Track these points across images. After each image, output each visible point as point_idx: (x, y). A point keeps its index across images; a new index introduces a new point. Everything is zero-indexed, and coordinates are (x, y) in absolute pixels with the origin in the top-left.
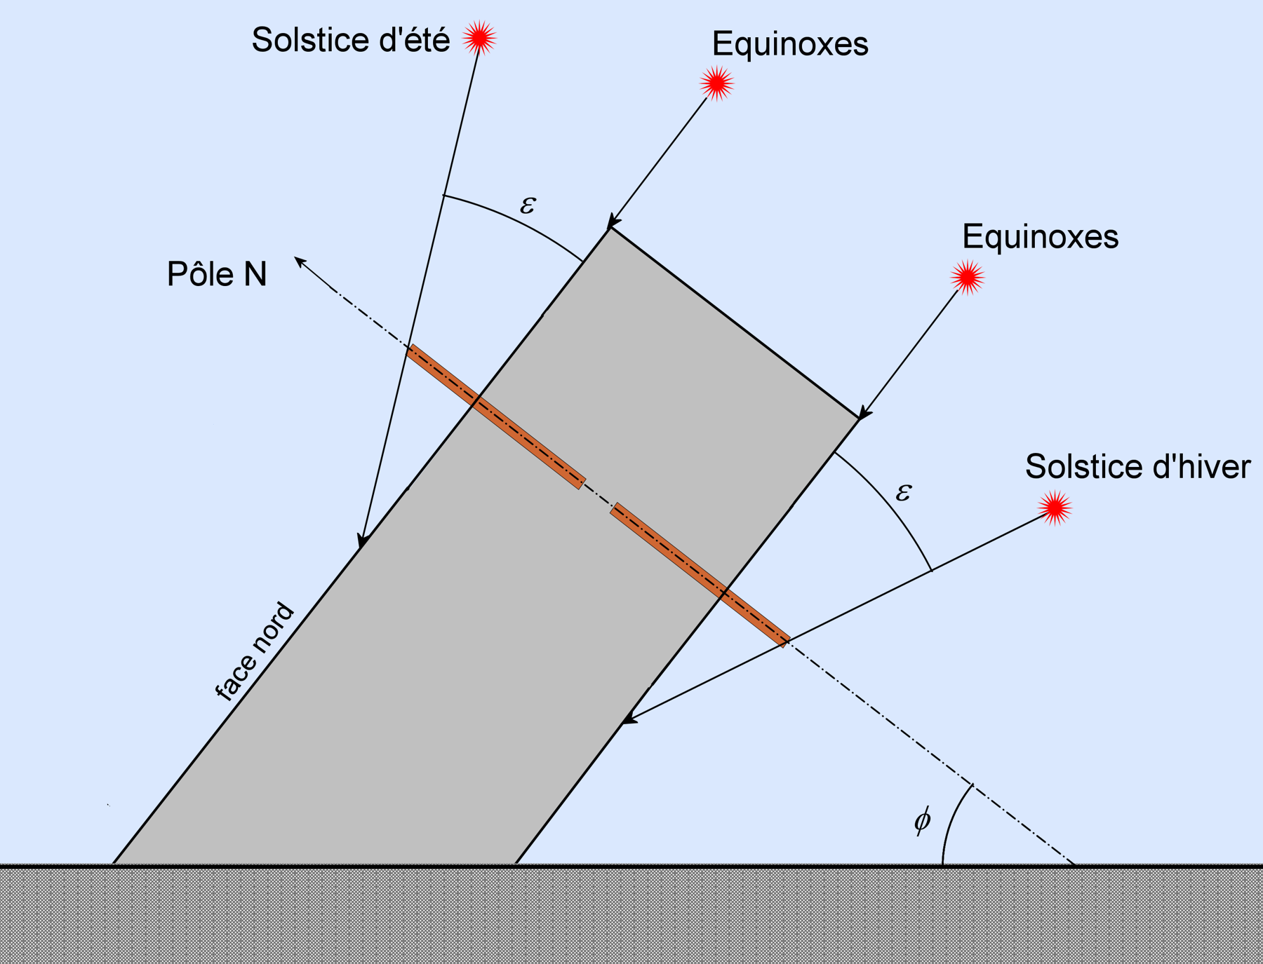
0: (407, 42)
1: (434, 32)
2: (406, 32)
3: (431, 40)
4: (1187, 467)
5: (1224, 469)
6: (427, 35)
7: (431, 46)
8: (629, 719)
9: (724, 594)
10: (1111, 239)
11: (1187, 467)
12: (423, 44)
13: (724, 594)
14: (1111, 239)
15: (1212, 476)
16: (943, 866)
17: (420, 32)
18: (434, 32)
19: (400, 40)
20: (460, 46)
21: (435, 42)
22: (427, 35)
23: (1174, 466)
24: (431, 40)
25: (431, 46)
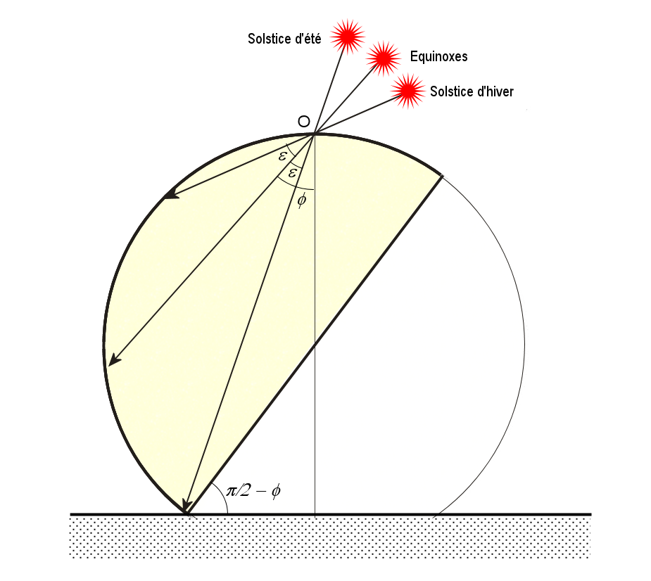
0: (306, 39)
1: (315, 35)
2: (305, 35)
3: (314, 39)
4: (490, 92)
5: (504, 92)
6: (313, 36)
7: (314, 41)
8: (171, 194)
9: (296, 187)
10: (254, 39)
11: (490, 92)
12: (311, 41)
13: (296, 187)
14: (254, 39)
15: (499, 96)
16: (315, 515)
17: (310, 35)
18: (315, 35)
19: (303, 38)
20: (330, 45)
21: (316, 39)
22: (313, 36)
23: (485, 91)
24: (314, 39)
25: (314, 41)
